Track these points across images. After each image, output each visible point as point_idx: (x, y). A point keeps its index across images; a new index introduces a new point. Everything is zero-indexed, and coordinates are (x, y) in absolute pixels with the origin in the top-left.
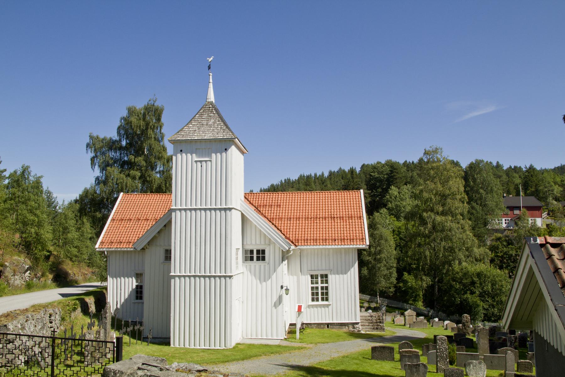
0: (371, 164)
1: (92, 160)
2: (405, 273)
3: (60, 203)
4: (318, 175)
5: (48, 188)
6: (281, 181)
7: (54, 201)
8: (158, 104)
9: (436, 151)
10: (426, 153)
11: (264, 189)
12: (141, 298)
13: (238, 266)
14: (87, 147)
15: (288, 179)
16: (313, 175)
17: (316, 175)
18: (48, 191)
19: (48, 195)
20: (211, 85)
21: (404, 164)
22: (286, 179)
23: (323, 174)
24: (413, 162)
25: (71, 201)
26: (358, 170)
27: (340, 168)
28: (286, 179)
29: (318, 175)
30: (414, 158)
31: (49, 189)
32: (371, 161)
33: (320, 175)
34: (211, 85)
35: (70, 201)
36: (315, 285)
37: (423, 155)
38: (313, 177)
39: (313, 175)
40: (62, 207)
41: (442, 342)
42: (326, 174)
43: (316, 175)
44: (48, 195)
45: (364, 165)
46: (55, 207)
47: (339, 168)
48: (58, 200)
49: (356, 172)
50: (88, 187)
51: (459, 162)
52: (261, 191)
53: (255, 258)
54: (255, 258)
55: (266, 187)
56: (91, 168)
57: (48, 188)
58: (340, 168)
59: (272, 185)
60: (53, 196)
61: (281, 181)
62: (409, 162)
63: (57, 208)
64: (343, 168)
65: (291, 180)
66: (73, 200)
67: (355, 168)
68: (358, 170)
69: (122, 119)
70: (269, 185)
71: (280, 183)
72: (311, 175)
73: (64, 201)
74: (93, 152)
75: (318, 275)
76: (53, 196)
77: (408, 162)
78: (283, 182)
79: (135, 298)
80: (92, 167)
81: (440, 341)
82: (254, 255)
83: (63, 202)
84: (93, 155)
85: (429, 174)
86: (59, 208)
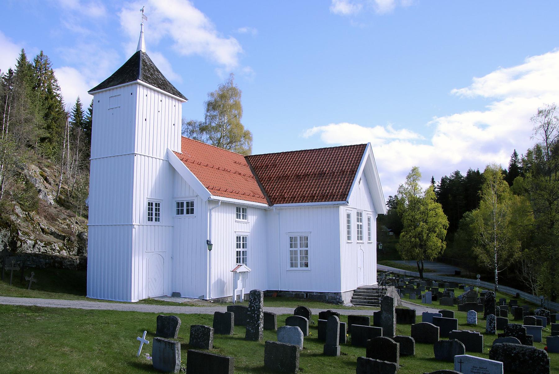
36: (293, 249)
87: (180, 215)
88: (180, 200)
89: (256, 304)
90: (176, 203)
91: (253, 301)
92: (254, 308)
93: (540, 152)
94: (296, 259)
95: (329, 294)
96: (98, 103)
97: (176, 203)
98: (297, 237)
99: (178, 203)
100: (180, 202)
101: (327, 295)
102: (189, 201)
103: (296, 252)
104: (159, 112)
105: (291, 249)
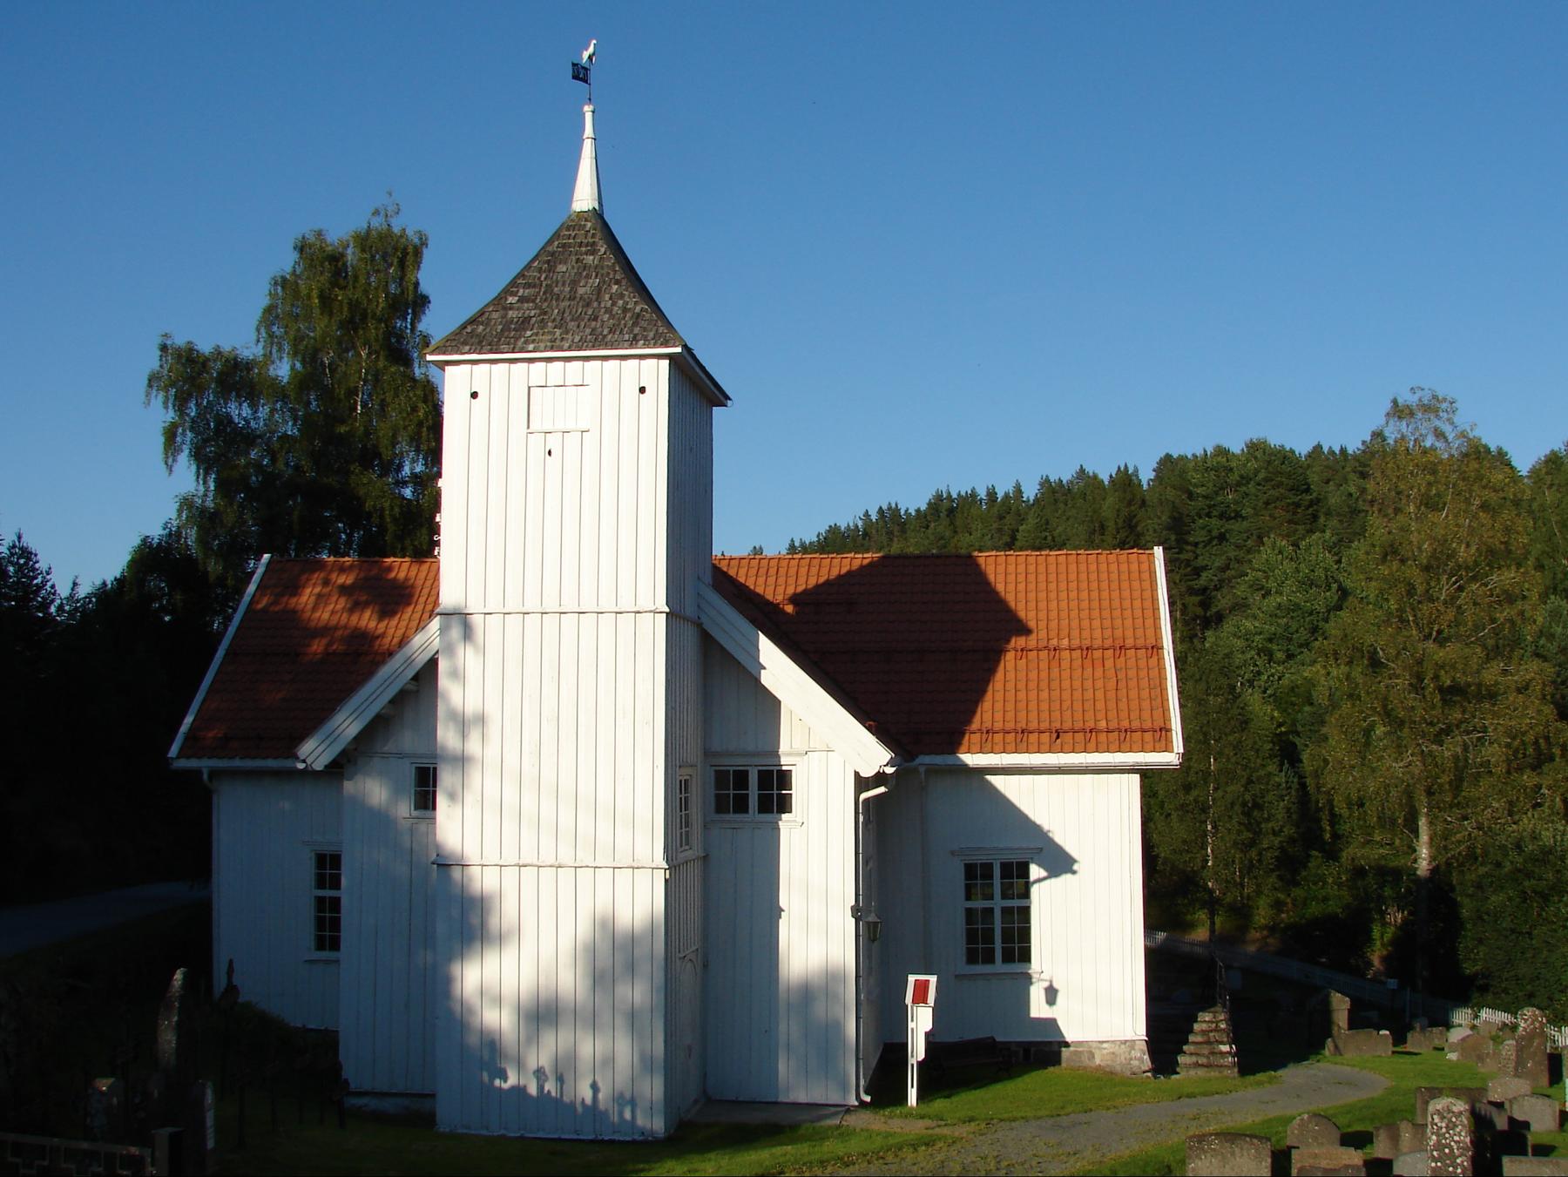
0: (1195, 456)
1: (170, 435)
2: (1314, 853)
3: (63, 591)
4: (1000, 495)
5: (19, 537)
6: (867, 514)
7: (44, 583)
8: (407, 224)
9: (1431, 407)
10: (1399, 411)
11: (803, 545)
12: (335, 944)
13: (687, 832)
14: (150, 386)
15: (890, 508)
16: (982, 494)
17: (992, 494)
18: (21, 549)
19: (22, 561)
20: (588, 149)
21: (1309, 456)
22: (885, 507)
23: (1018, 490)
24: (1343, 451)
25: (104, 584)
26: (1146, 475)
27: (1082, 470)
28: (885, 507)
29: (1000, 495)
30: (1351, 437)
31: (26, 541)
32: (1192, 443)
33: (1007, 496)
34: (588, 149)
35: (98, 582)
36: (979, 904)
37: (1383, 421)
38: (981, 500)
39: (982, 494)
40: (67, 608)
41: (1450, 1121)
42: (1030, 492)
43: (992, 494)
44: (22, 561)
45: (1168, 456)
46: (45, 605)
47: (1317, 443)
48: (54, 578)
49: (1140, 485)
50: (156, 532)
51: (1506, 454)
52: (792, 548)
53: (753, 802)
54: (753, 802)
55: (810, 537)
56: (163, 463)
57: (19, 537)
58: (1082, 470)
59: (834, 530)
60: (37, 566)
61: (867, 514)
62: (1332, 452)
63: (53, 609)
64: (1090, 470)
65: (902, 512)
66: (109, 583)
67: (1136, 470)
68: (1146, 475)
69: (276, 284)
70: (823, 529)
71: (860, 524)
72: (973, 495)
73: (75, 584)
74: (170, 405)
75: (991, 865)
76: (37, 566)
77: (1326, 450)
78: (874, 518)
79: (312, 944)
80: (166, 463)
81: (1443, 1118)
82: (757, 792)
83: (73, 589)
84: (171, 415)
85: (347, 350)
86: (60, 608)
87: (731, 816)
88: (733, 763)
89: (1456, 1138)
90: (416, 768)
91: (1444, 1130)
92: (1452, 1150)
93: (29, 559)
94: (988, 936)
95: (1105, 1045)
96: (1409, 389)
97: (416, 768)
98: (992, 864)
99: (419, 768)
100: (731, 769)
101: (1100, 1049)
102: (728, 768)
103: (989, 912)
104: (550, 453)
105: (970, 904)
